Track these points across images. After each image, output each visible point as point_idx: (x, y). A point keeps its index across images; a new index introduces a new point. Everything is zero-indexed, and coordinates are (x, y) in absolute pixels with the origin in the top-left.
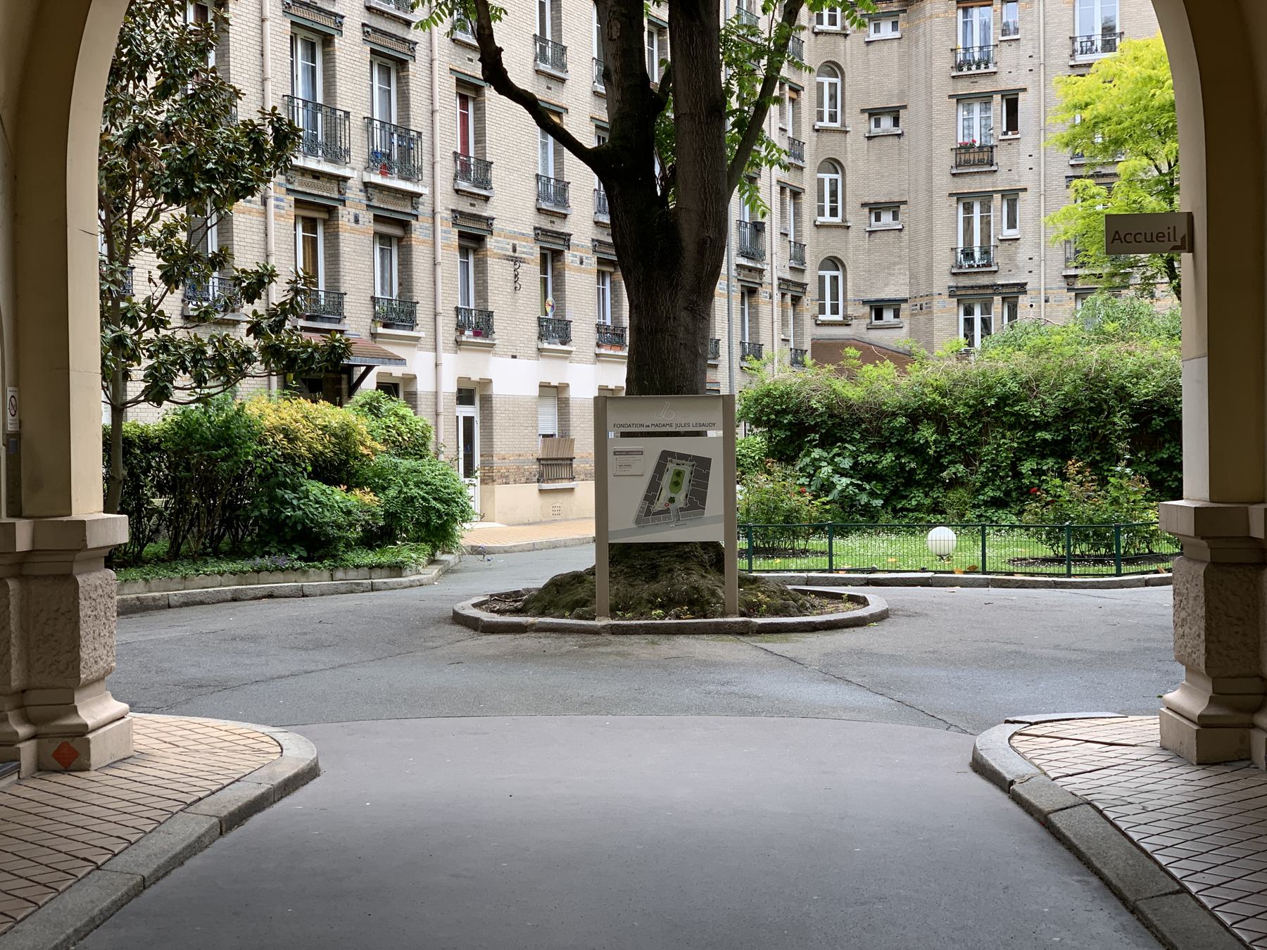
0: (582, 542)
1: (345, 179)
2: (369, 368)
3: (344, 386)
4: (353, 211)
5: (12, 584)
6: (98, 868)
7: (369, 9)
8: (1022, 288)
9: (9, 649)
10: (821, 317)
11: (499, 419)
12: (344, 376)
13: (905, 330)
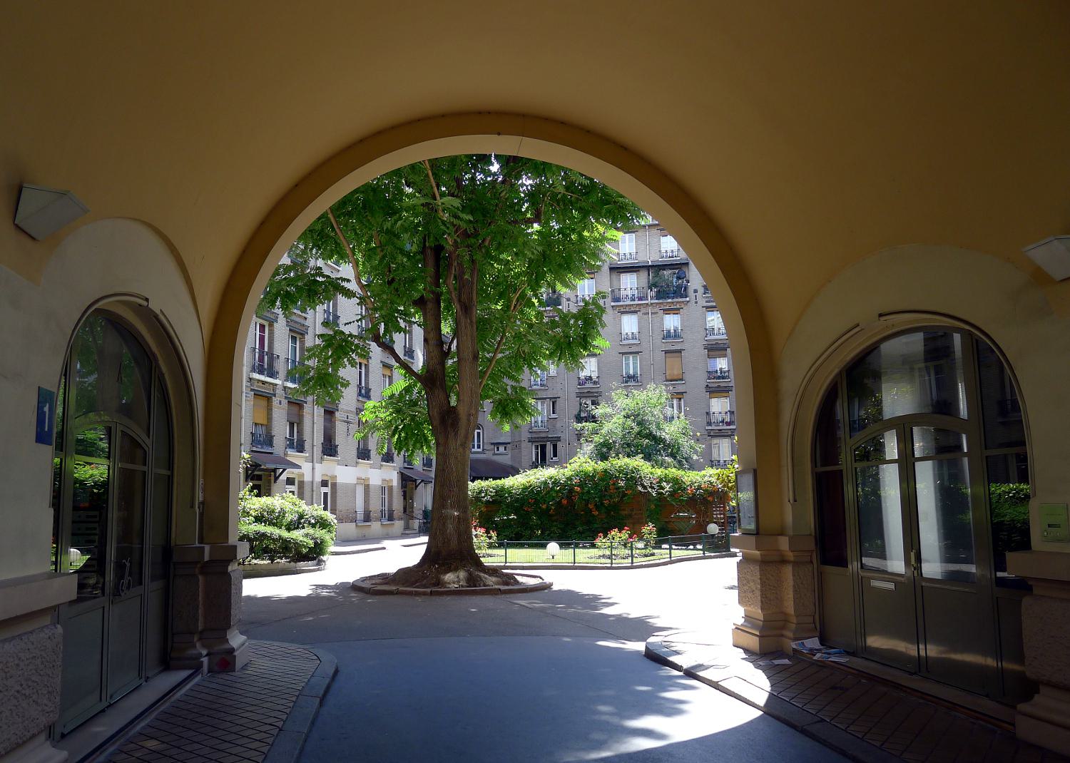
0: (927, 561)
1: (276, 385)
2: (284, 470)
3: (273, 478)
4: (279, 399)
5: (201, 578)
6: (280, 730)
7: (161, 310)
8: (559, 439)
9: (198, 610)
10: (473, 450)
11: (339, 493)
12: (272, 473)
13: (510, 456)
